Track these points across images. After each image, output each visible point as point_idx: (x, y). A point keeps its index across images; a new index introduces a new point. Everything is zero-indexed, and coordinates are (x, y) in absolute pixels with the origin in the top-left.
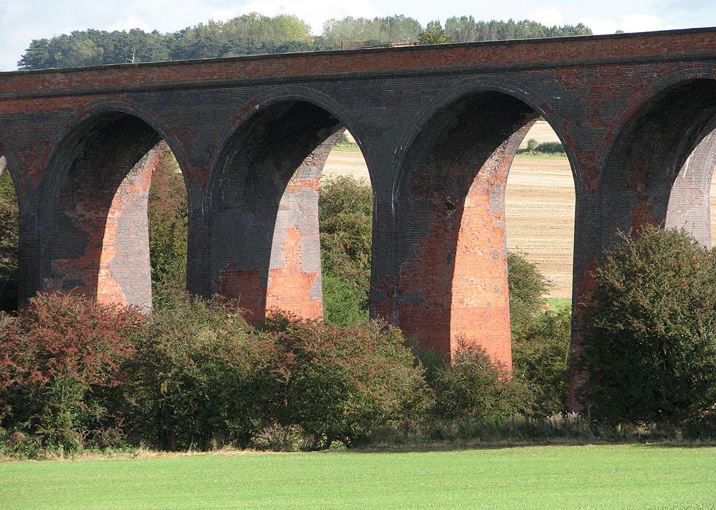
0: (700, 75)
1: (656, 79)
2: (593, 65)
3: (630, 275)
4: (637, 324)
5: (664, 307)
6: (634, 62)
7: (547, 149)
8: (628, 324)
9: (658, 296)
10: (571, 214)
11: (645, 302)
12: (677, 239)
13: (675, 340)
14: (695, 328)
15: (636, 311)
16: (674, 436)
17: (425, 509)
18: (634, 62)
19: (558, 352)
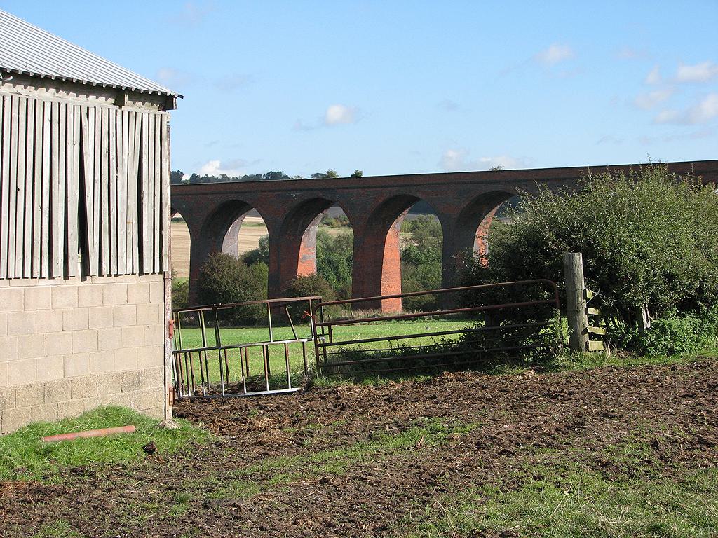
0: (234, 199)
1: (395, 191)
2: (196, 195)
3: (213, 269)
4: (215, 286)
5: (224, 281)
6: (211, 194)
7: (261, 224)
8: (212, 286)
9: (223, 277)
10: (189, 246)
11: (218, 279)
12: (228, 257)
13: (228, 291)
14: (235, 287)
15: (215, 282)
16: (228, 325)
17: (485, 537)
18: (211, 194)
19: (183, 297)
